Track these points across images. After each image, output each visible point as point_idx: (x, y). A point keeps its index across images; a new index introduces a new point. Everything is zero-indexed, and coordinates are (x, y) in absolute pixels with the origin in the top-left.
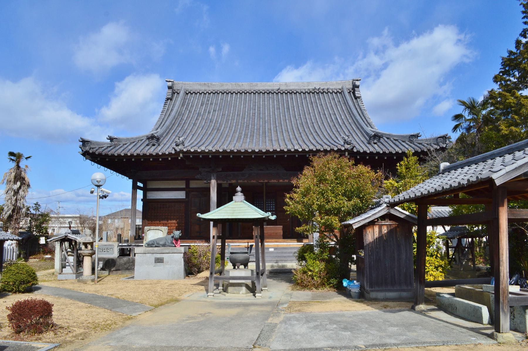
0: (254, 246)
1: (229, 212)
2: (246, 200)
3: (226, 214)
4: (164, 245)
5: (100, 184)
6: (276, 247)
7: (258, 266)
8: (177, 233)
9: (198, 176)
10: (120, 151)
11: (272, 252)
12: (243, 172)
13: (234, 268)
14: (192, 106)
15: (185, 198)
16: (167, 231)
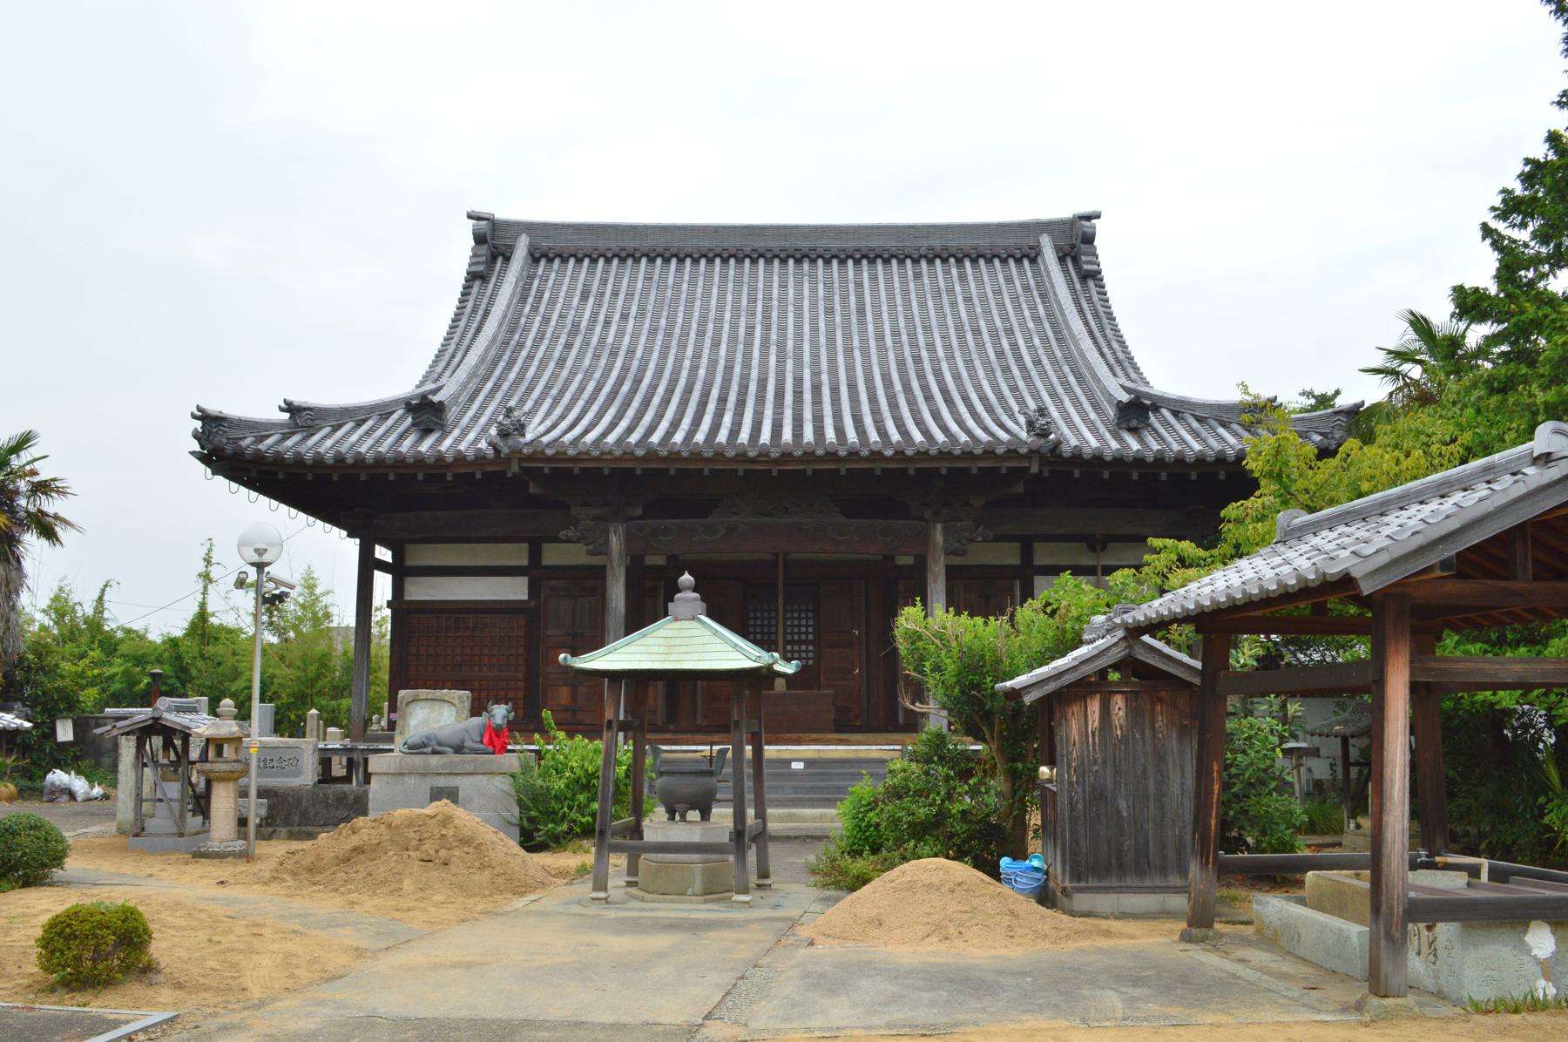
0: (729, 755)
1: (655, 649)
2: (708, 615)
3: (644, 657)
4: (459, 749)
5: (265, 558)
6: (810, 755)
7: (739, 816)
8: (500, 712)
9: (570, 532)
10: (324, 444)
11: (796, 774)
12: (710, 520)
13: (672, 818)
14: (552, 302)
15: (525, 597)
16: (467, 704)
